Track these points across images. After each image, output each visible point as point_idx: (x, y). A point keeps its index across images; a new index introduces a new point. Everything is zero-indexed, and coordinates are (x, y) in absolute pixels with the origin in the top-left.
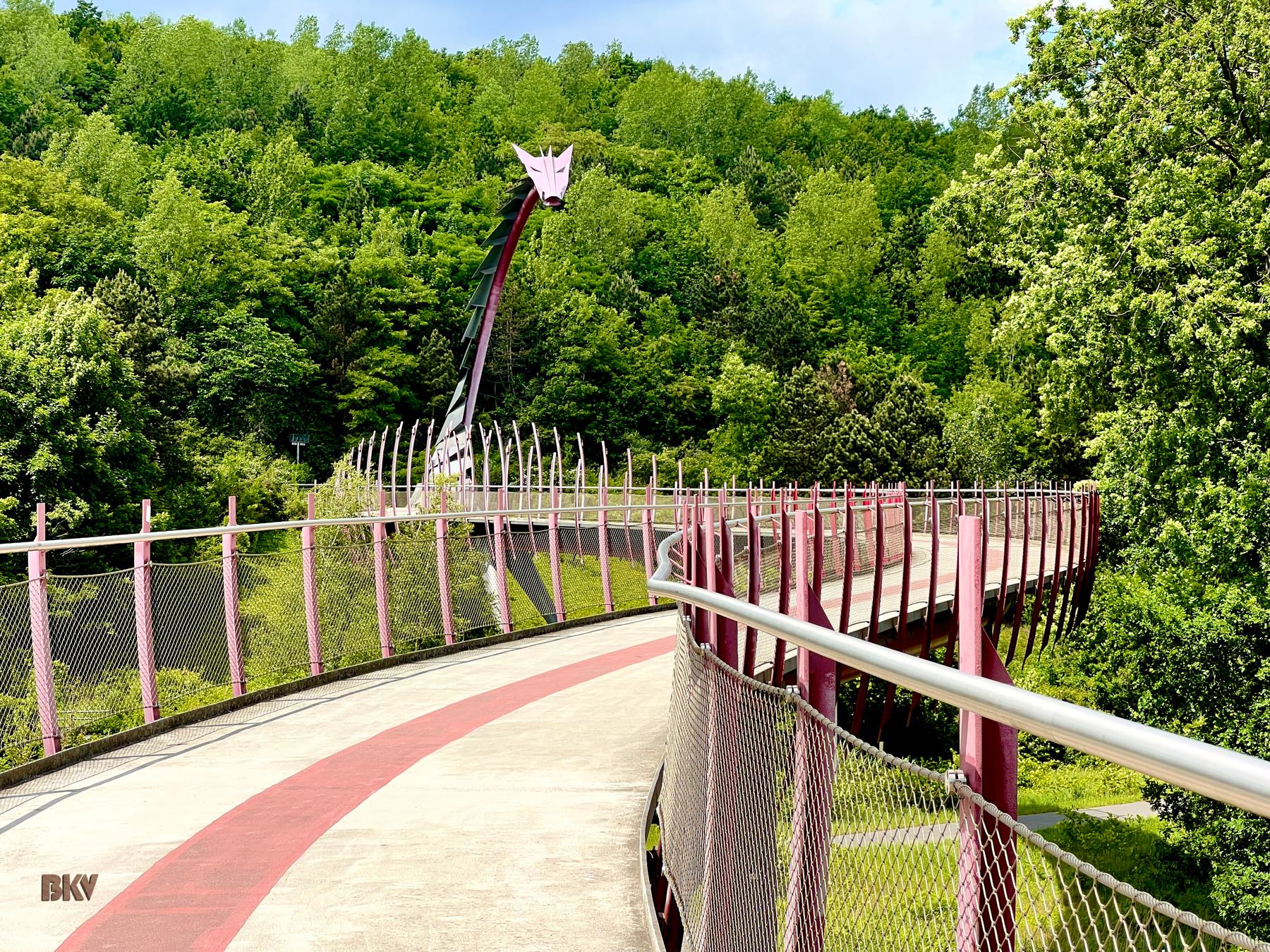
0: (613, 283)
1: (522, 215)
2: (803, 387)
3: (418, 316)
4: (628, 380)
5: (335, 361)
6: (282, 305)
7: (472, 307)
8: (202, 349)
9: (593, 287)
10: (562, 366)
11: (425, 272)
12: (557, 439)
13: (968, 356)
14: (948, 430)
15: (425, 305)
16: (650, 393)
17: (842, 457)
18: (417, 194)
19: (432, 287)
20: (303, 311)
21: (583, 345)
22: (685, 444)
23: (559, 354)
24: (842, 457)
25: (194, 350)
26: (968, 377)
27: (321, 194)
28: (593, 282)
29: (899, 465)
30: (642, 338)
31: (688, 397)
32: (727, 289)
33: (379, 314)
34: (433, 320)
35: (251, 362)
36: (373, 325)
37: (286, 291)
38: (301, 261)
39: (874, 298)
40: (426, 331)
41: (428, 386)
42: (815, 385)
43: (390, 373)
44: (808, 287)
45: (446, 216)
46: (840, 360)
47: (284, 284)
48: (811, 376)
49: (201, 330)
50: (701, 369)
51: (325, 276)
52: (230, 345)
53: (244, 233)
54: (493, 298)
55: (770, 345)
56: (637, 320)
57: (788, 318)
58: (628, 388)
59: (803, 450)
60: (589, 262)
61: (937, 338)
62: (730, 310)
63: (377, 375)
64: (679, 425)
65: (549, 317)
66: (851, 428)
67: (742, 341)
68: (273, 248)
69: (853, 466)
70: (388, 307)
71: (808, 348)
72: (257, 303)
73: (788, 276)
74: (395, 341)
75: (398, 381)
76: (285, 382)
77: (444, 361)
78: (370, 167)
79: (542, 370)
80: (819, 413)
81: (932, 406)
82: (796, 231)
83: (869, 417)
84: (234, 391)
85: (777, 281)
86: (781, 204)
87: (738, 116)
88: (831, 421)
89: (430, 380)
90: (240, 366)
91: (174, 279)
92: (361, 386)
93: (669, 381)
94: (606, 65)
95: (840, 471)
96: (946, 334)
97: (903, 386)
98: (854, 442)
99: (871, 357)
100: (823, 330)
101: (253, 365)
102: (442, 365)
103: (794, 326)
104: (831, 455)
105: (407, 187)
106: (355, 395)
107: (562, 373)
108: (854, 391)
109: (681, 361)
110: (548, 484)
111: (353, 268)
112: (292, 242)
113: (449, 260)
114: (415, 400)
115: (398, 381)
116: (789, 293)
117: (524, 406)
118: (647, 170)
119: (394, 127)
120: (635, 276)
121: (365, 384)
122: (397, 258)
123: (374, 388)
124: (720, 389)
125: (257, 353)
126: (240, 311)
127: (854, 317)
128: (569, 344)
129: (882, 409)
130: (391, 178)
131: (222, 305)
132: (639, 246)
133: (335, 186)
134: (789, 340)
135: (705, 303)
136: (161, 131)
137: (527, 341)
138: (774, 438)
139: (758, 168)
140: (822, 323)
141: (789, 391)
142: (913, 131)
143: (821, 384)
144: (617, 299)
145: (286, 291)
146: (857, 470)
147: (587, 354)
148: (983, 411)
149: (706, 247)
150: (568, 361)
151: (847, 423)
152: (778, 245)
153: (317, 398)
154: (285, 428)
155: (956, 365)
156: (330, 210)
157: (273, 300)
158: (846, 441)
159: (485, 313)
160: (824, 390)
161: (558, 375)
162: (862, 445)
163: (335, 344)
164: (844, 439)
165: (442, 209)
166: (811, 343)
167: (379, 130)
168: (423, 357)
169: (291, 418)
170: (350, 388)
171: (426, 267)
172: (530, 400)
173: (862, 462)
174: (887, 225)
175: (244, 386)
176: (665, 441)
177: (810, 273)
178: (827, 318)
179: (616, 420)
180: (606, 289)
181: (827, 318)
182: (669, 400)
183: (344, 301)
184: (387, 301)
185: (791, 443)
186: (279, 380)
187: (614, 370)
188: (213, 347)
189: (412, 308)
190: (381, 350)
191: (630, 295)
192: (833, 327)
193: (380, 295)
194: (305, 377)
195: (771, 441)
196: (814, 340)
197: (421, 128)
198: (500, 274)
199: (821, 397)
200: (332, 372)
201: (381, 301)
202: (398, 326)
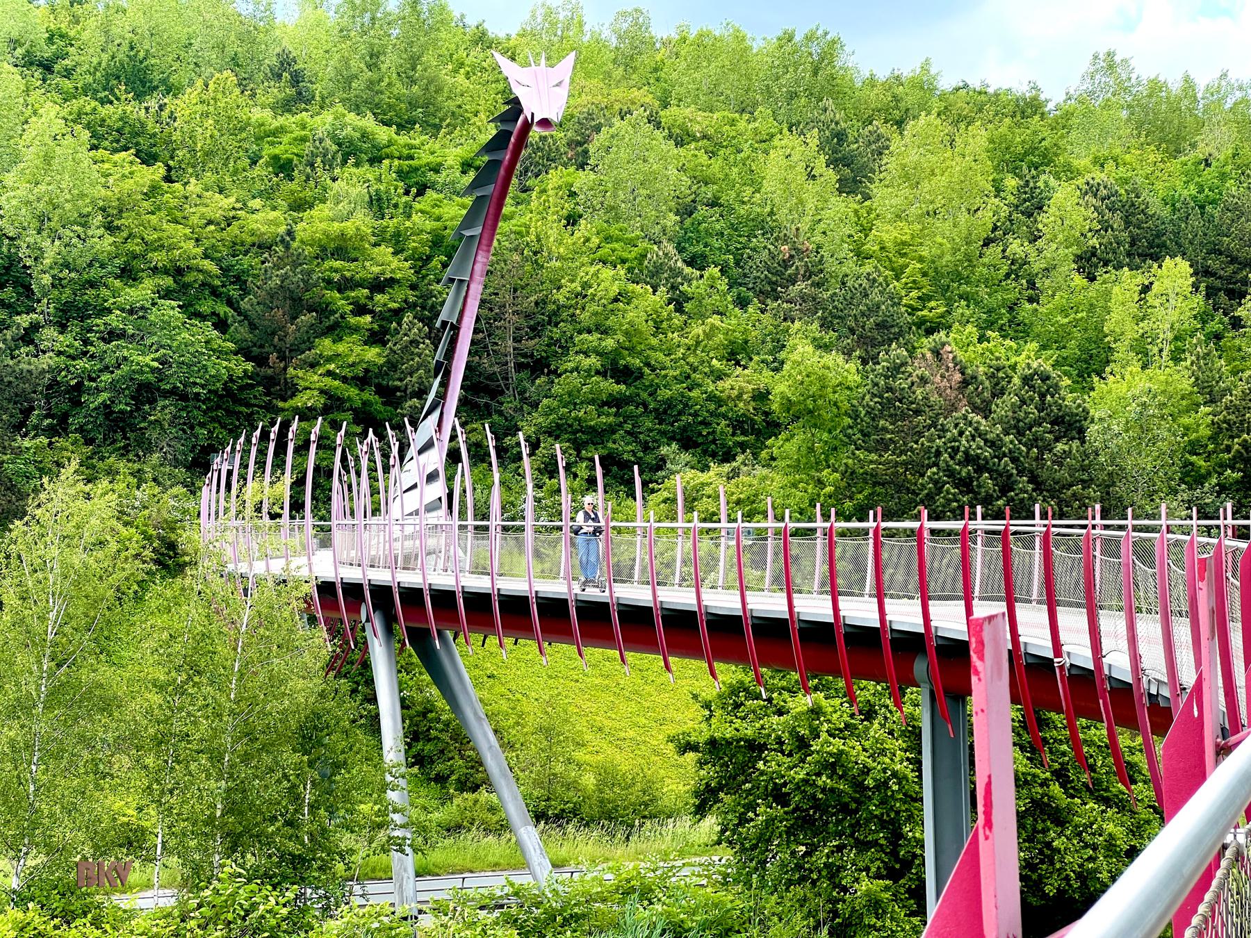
0: (649, 256)
2: (894, 377)
4: (666, 376)
7: (452, 281)
8: (86, 342)
9: (623, 261)
11: (398, 242)
12: (491, 444)
13: (1109, 342)
14: (1093, 430)
15: (392, 282)
17: (951, 473)
18: (405, 152)
19: (406, 260)
20: (234, 292)
21: (606, 332)
22: (740, 458)
24: (951, 473)
25: (76, 344)
26: (1108, 369)
27: (277, 150)
28: (625, 255)
29: (1029, 482)
31: (745, 397)
34: (405, 301)
35: (153, 360)
36: (323, 310)
37: (208, 265)
38: (234, 229)
39: (985, 271)
40: (398, 313)
41: (398, 389)
42: (910, 375)
43: (347, 372)
44: (901, 261)
45: (441, 178)
46: (943, 344)
47: (206, 256)
48: (904, 364)
49: (89, 317)
51: (264, 247)
52: (122, 335)
53: (153, 191)
54: (478, 267)
55: (852, 331)
56: (679, 302)
57: (875, 296)
58: (665, 387)
59: (897, 464)
61: (1066, 320)
62: (801, 286)
63: (329, 373)
64: (734, 434)
66: (961, 433)
67: (816, 325)
68: (196, 215)
69: (965, 485)
70: (345, 285)
72: (168, 281)
73: (876, 248)
74: (356, 329)
75: (362, 381)
76: (203, 386)
80: (917, 412)
81: (1070, 400)
82: (885, 197)
83: (986, 418)
84: (133, 398)
85: (861, 256)
88: (934, 425)
90: (138, 364)
91: (51, 252)
92: (306, 389)
93: (719, 376)
94: (672, 45)
95: (948, 492)
96: (1080, 315)
97: (1032, 376)
98: (966, 453)
99: (985, 344)
100: (920, 313)
101: (156, 364)
102: (417, 359)
104: (934, 469)
106: (299, 401)
108: (965, 383)
109: (736, 354)
110: (485, 517)
111: (300, 235)
112: (221, 204)
113: (429, 225)
114: (380, 407)
115: (362, 381)
116: (876, 267)
117: (529, 413)
118: (705, 137)
119: (400, 89)
121: (313, 387)
122: (362, 222)
124: (781, 388)
125: (162, 347)
126: (141, 292)
127: (961, 297)
129: (1003, 407)
131: (118, 283)
132: (686, 211)
133: (295, 139)
136: (115, 95)
137: (533, 328)
138: (857, 449)
139: (837, 123)
140: (918, 305)
141: (876, 384)
142: (1018, 106)
143: (919, 372)
144: (653, 276)
145: (208, 265)
146: (971, 490)
147: (609, 343)
148: (1144, 405)
149: (771, 213)
151: (956, 425)
152: (863, 212)
153: (248, 405)
155: (1091, 357)
156: (283, 167)
157: (189, 278)
158: (956, 450)
159: (468, 286)
160: (923, 381)
161: (571, 372)
162: (978, 457)
164: (952, 448)
165: (436, 170)
166: (905, 328)
167: (382, 93)
168: (391, 349)
170: (291, 390)
171: (397, 234)
172: (535, 405)
173: (977, 479)
174: (998, 191)
175: (145, 393)
176: (714, 455)
177: (904, 243)
178: (924, 299)
179: (650, 430)
181: (924, 299)
182: (719, 402)
183: (284, 278)
184: (343, 277)
186: (195, 384)
187: (648, 365)
188: (103, 339)
189: (379, 285)
190: (334, 342)
191: (671, 269)
192: (936, 308)
193: (336, 271)
197: (432, 88)
198: (486, 236)
200: (270, 371)
201: (336, 277)
202: (360, 310)
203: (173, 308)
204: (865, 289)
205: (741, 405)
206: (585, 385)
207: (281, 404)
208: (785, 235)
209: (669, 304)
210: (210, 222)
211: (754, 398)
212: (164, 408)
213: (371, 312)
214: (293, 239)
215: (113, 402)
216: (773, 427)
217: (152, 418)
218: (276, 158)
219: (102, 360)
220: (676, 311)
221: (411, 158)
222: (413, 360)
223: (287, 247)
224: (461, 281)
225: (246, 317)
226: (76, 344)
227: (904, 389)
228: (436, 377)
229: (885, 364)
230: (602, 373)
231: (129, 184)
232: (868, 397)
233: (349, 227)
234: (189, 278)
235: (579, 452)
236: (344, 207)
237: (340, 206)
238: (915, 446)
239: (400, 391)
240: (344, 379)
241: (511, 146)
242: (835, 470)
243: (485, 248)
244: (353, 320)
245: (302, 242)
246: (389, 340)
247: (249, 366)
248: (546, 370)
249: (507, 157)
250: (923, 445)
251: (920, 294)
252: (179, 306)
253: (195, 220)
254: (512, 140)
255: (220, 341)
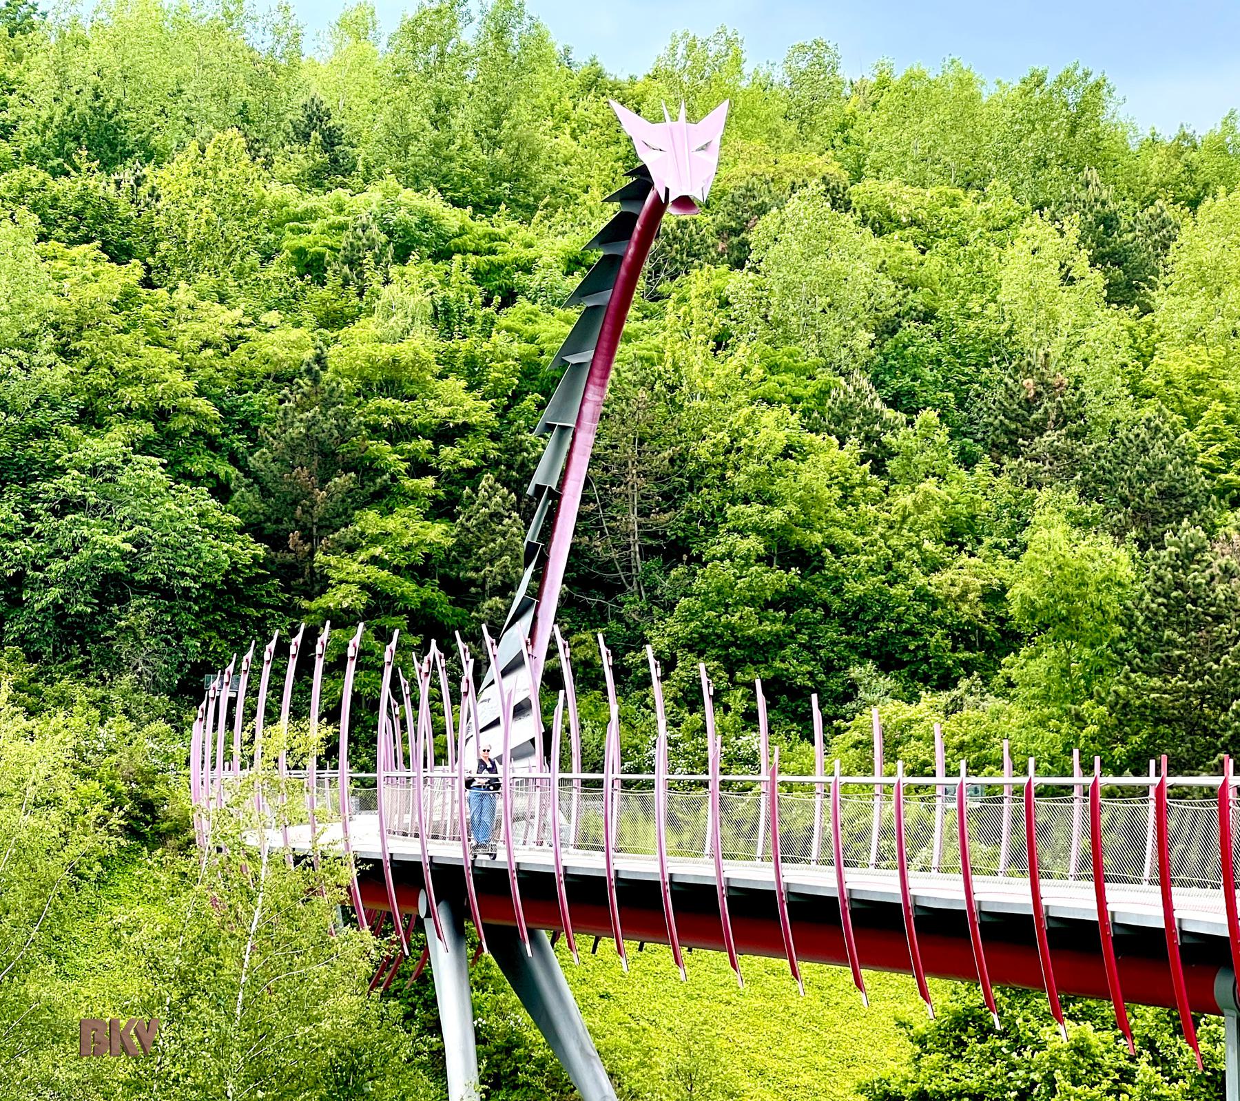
0: (833, 393)
1: (638, 244)
3: (458, 450)
5: (294, 536)
6: (197, 433)
7: (550, 428)
8: (30, 516)
9: (797, 400)
10: (730, 540)
11: (474, 374)
15: (465, 429)
16: (896, 591)
18: (485, 245)
20: (239, 443)
22: (964, 684)
23: (725, 521)
25: (16, 517)
27: (303, 241)
28: (798, 391)
30: (887, 490)
31: (971, 596)
32: (1048, 404)
33: (380, 447)
35: (124, 541)
36: (367, 469)
37: (204, 406)
38: (241, 354)
40: (472, 475)
41: (472, 582)
42: (1209, 566)
44: (1196, 401)
45: (533, 281)
47: (200, 393)
49: (35, 479)
50: (997, 546)
53: (125, 301)
54: (588, 409)
55: (1125, 501)
56: (877, 460)
57: (1159, 451)
60: (791, 356)
63: (374, 560)
64: (954, 649)
65: (703, 451)
70: (399, 433)
71: (1195, 506)
73: (1161, 382)
74: (413, 497)
75: (420, 572)
76: (195, 579)
77: (504, 535)
78: (397, 192)
79: (694, 552)
80: (1219, 619)
86: (1142, 266)
87: (1072, 133)
89: (477, 570)
92: (341, 582)
93: (935, 567)
100: (1222, 476)
101: (128, 547)
102: (500, 540)
103: (1170, 467)
105: (463, 231)
106: (330, 600)
107: (729, 555)
110: (598, 767)
113: (518, 348)
114: (446, 609)
115: (420, 572)
116: (1159, 410)
119: (477, 154)
120: (878, 384)
121: (350, 579)
123: (364, 587)
128: (747, 501)
130: (433, 212)
132: (889, 329)
133: (330, 227)
134: (1161, 493)
135: (1007, 432)
137: (666, 496)
138: (1133, 671)
141: (1160, 579)
145: (204, 406)
147: (776, 516)
149: (1010, 333)
150: (742, 532)
153: (258, 605)
154: (194, 664)
157: (176, 424)
163: (295, 503)
165: (527, 269)
169: (205, 644)
170: (320, 584)
172: (670, 607)
176: (926, 679)
179: (834, 643)
180: (822, 404)
182: (934, 603)
185: (1166, 681)
186: (183, 575)
188: (54, 511)
189: (445, 434)
190: (382, 514)
193: (380, 411)
194: (235, 568)
195: (1128, 678)
196: (1208, 494)
199: (1220, 588)
201: (386, 421)
202: (419, 469)
203: (153, 467)
204: (1143, 441)
205: (965, 608)
206: (740, 577)
207: (305, 604)
208: (1029, 364)
209: (863, 462)
210: (206, 345)
211: (984, 598)
212: (139, 609)
213: (435, 472)
214: (324, 368)
215: (67, 601)
216: (1011, 639)
217: (123, 623)
218: (300, 252)
219: (52, 541)
220: (873, 471)
221: (494, 252)
222: (494, 541)
223: (316, 380)
224: (564, 429)
225: (257, 480)
226: (16, 517)
227: (1200, 585)
228: (527, 565)
229: (1173, 549)
230: (766, 560)
231: (91, 291)
232: (1147, 597)
233: (404, 352)
234: (176, 424)
235: (732, 674)
236: (397, 322)
237: (392, 321)
238: (1215, 667)
239: (476, 586)
240: (396, 570)
241: (635, 235)
242: (1101, 702)
243: (597, 381)
244: (409, 483)
245: (336, 372)
246: (460, 513)
247: (260, 550)
248: (685, 557)
249: (631, 251)
250: (1226, 664)
251: (1223, 449)
252: (162, 465)
253: (184, 341)
254: (638, 226)
255: (217, 513)
